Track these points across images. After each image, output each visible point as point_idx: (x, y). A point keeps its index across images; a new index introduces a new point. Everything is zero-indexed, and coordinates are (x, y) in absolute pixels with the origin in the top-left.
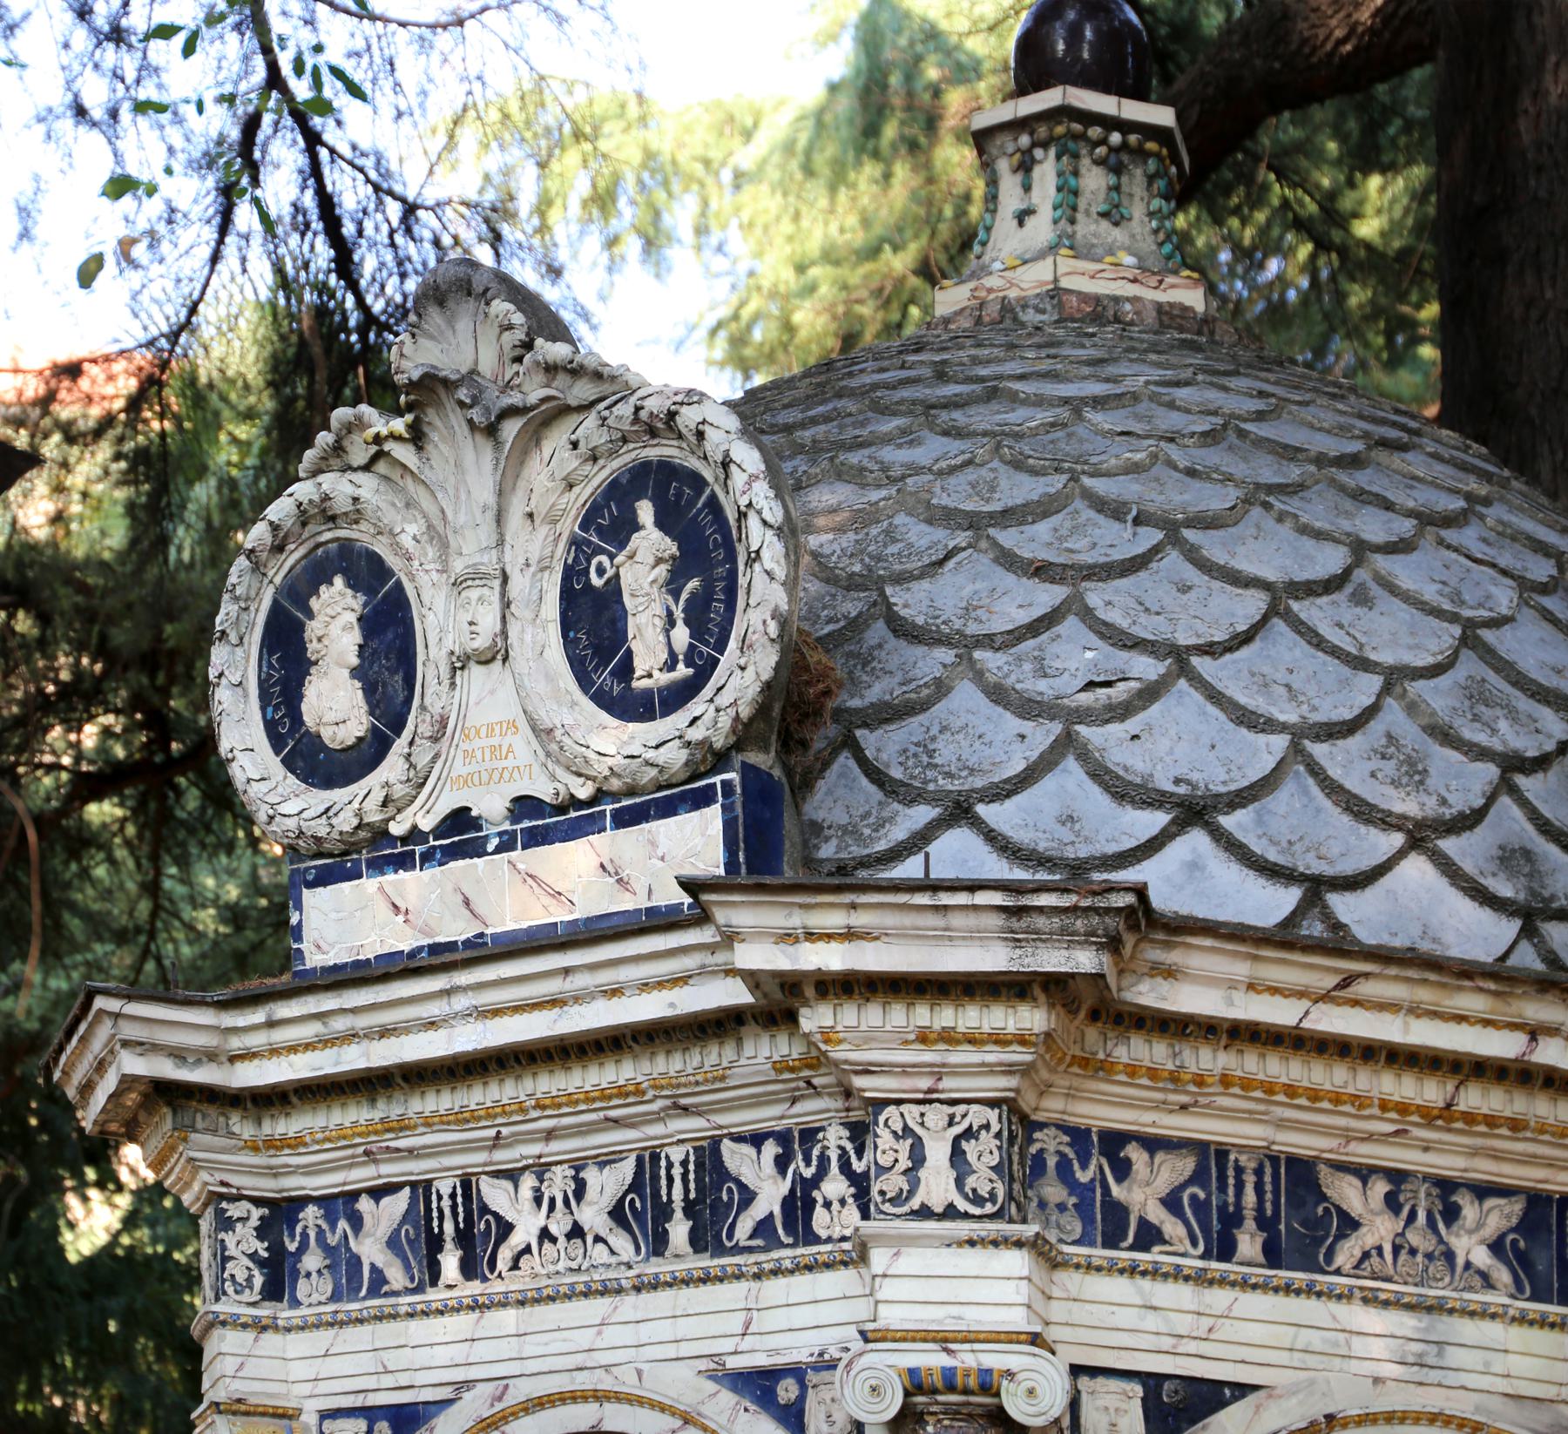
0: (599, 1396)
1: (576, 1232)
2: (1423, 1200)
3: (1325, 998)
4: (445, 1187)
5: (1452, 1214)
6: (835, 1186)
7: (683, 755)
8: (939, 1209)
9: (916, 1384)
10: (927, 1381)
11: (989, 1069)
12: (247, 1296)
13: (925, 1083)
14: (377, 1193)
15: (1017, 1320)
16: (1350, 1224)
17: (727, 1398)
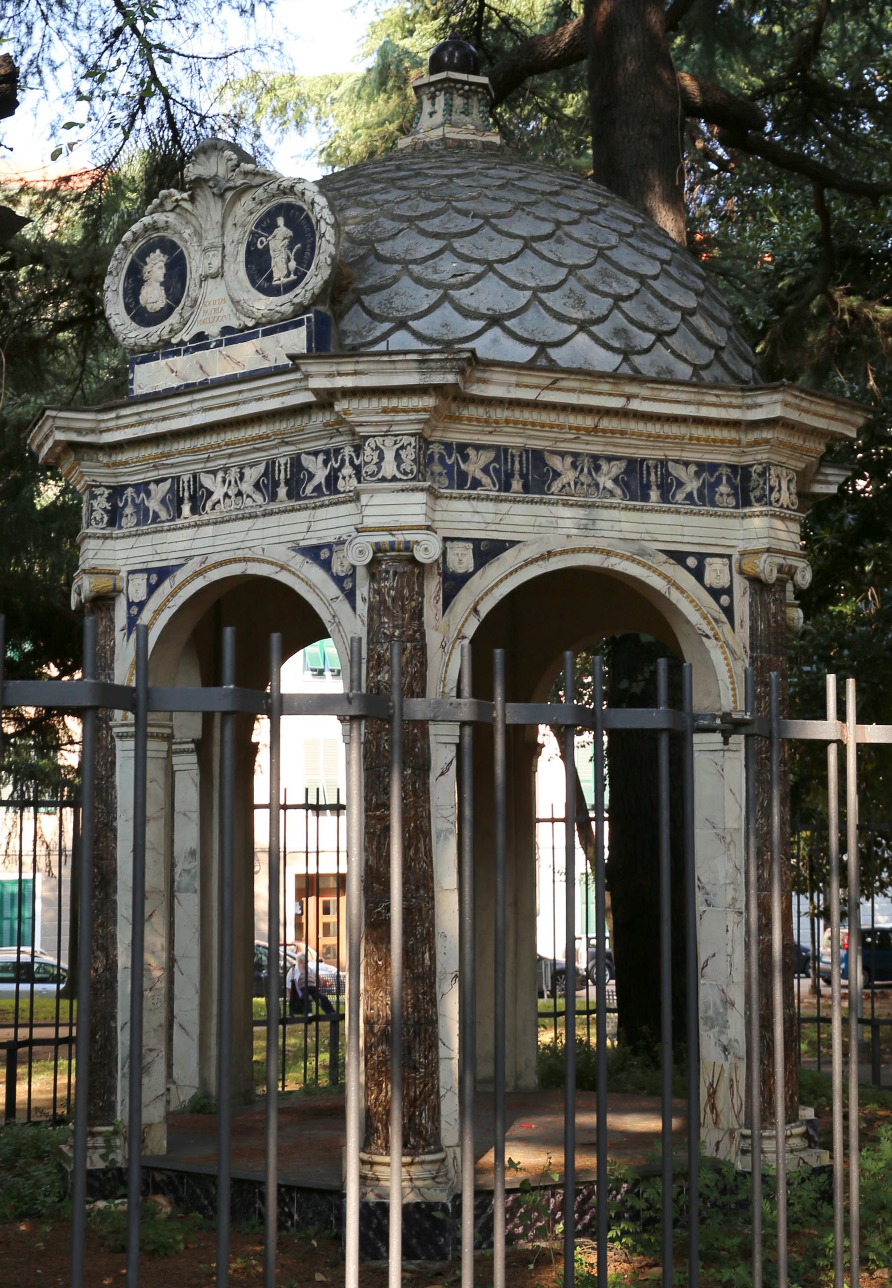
0: (246, 560)
1: (239, 494)
2: (586, 464)
3: (547, 388)
4: (186, 479)
5: (598, 468)
6: (347, 470)
7: (291, 308)
9: (378, 548)
11: (411, 422)
12: (101, 526)
13: (385, 429)
14: (158, 482)
15: (421, 520)
17: (300, 558)
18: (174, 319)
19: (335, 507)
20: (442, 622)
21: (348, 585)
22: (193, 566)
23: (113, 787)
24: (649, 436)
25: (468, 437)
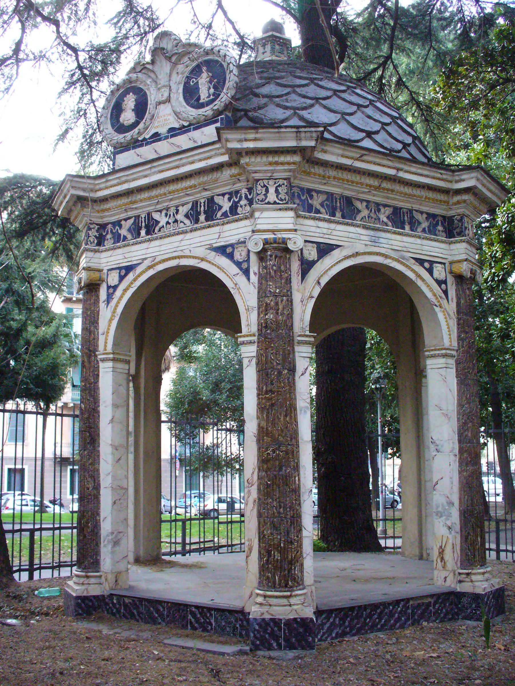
0: (179, 257)
1: (176, 221)
2: (373, 207)
3: (357, 159)
4: (143, 216)
5: (379, 210)
6: (243, 202)
7: (212, 113)
8: (272, 202)
9: (266, 242)
10: (269, 241)
11: (285, 171)
12: (93, 245)
13: (269, 175)
14: (126, 220)
15: (291, 226)
16: (359, 211)
17: (213, 253)
18: (141, 126)
19: (236, 223)
20: (301, 287)
21: (245, 266)
22: (147, 263)
23: (98, 388)
24: (406, 194)
25: (313, 185)
